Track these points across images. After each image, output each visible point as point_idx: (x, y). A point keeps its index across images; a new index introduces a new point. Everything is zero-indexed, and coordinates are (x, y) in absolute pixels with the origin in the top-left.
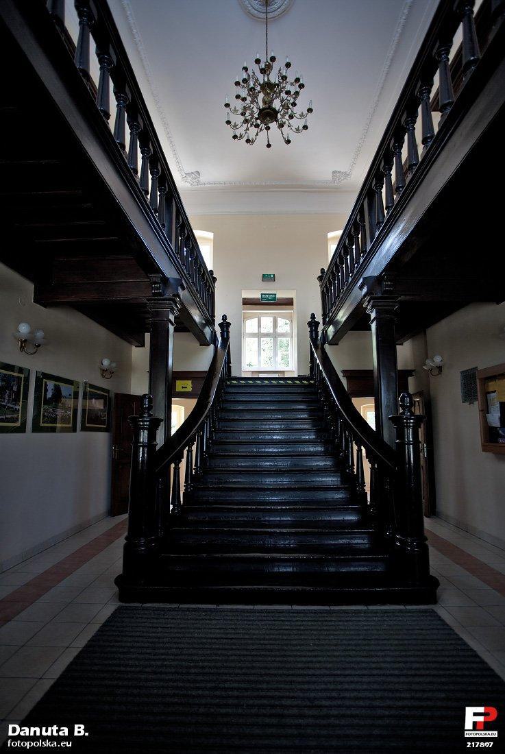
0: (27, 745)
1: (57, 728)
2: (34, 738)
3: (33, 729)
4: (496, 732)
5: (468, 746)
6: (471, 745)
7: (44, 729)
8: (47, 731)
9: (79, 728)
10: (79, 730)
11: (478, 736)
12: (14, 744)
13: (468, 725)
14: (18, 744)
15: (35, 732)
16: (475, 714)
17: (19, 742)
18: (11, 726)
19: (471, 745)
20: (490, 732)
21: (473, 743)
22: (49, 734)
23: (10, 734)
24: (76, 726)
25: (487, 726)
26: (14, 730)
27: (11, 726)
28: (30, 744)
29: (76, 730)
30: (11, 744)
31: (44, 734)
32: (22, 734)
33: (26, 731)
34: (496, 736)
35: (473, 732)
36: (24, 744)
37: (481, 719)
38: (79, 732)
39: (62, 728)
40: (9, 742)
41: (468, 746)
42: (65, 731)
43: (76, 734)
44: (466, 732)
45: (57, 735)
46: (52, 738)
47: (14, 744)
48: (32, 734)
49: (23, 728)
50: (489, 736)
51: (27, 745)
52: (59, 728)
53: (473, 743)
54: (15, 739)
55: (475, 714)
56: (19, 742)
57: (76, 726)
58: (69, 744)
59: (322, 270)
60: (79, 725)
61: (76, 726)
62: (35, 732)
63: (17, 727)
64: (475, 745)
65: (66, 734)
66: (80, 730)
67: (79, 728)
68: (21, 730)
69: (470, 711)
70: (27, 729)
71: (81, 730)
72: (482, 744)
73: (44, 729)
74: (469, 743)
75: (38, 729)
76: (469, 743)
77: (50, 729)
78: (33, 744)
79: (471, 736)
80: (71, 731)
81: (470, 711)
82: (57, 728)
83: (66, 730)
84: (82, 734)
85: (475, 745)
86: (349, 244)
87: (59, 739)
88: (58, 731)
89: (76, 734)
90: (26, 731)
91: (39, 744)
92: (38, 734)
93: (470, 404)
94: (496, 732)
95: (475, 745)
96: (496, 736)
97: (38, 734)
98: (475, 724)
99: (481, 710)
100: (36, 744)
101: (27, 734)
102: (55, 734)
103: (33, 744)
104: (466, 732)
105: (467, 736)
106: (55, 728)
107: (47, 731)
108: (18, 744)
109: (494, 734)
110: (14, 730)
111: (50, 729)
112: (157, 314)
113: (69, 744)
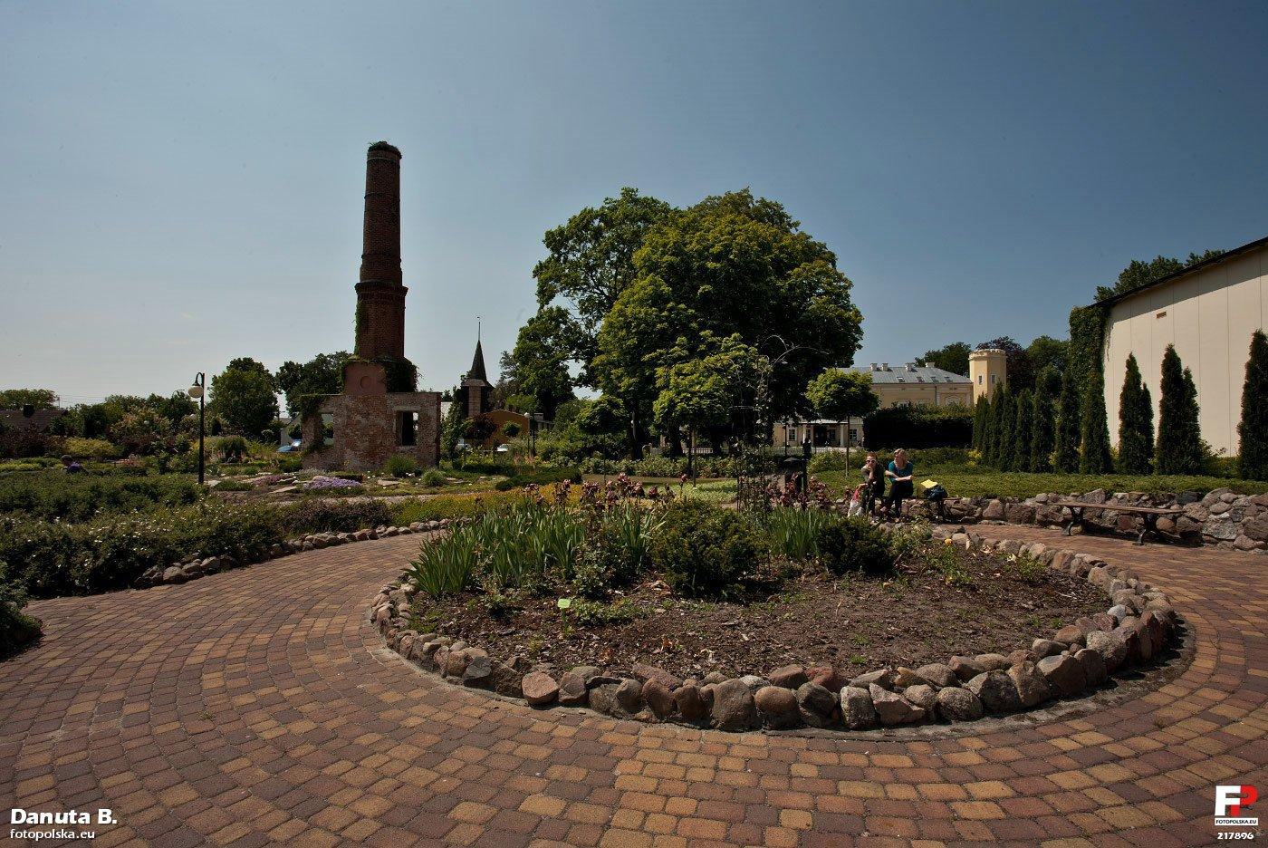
1: (76, 814)
2: (45, 826)
3: (43, 815)
4: (1257, 819)
6: (1224, 836)
7: (58, 815)
9: (105, 813)
10: (105, 816)
11: (1232, 824)
13: (1220, 810)
15: (46, 819)
16: (1229, 796)
17: (25, 832)
18: (14, 812)
19: (1224, 836)
20: (1249, 819)
21: (1226, 834)
22: (65, 821)
23: (14, 821)
24: (101, 811)
27: (14, 812)
28: (40, 835)
29: (101, 816)
30: (14, 834)
31: (58, 821)
32: (29, 821)
33: (34, 818)
34: (1257, 824)
36: (32, 835)
37: (1236, 802)
38: (105, 819)
39: (82, 814)
40: (12, 832)
42: (86, 818)
43: (100, 821)
44: (1216, 819)
45: (75, 822)
46: (68, 827)
47: (19, 835)
48: (42, 822)
49: (30, 814)
50: (1246, 824)
51: (36, 835)
52: (78, 815)
53: (1226, 834)
55: (1229, 796)
56: (25, 832)
57: (101, 811)
58: (91, 835)
59: (506, 353)
62: (46, 819)
64: (1229, 836)
65: (88, 822)
66: (105, 816)
67: (105, 813)
68: (27, 817)
69: (1221, 791)
70: (35, 815)
71: (107, 816)
72: (1238, 834)
73: (58, 815)
75: (50, 815)
76: (1221, 834)
77: (66, 815)
79: (1223, 824)
81: (1221, 791)
82: (76, 814)
83: (87, 816)
85: (1229, 836)
86: (712, 254)
87: (76, 828)
88: (76, 818)
89: (100, 821)
90: (34, 818)
92: (50, 821)
94: (1257, 819)
95: (1229, 836)
96: (1257, 824)
97: (50, 821)
98: (1228, 808)
99: (1236, 789)
100: (48, 835)
101: (36, 822)
102: (73, 821)
104: (1216, 819)
105: (1218, 824)
106: (73, 813)
109: (1253, 821)
110: (18, 816)
111: (66, 815)
113: (91, 835)
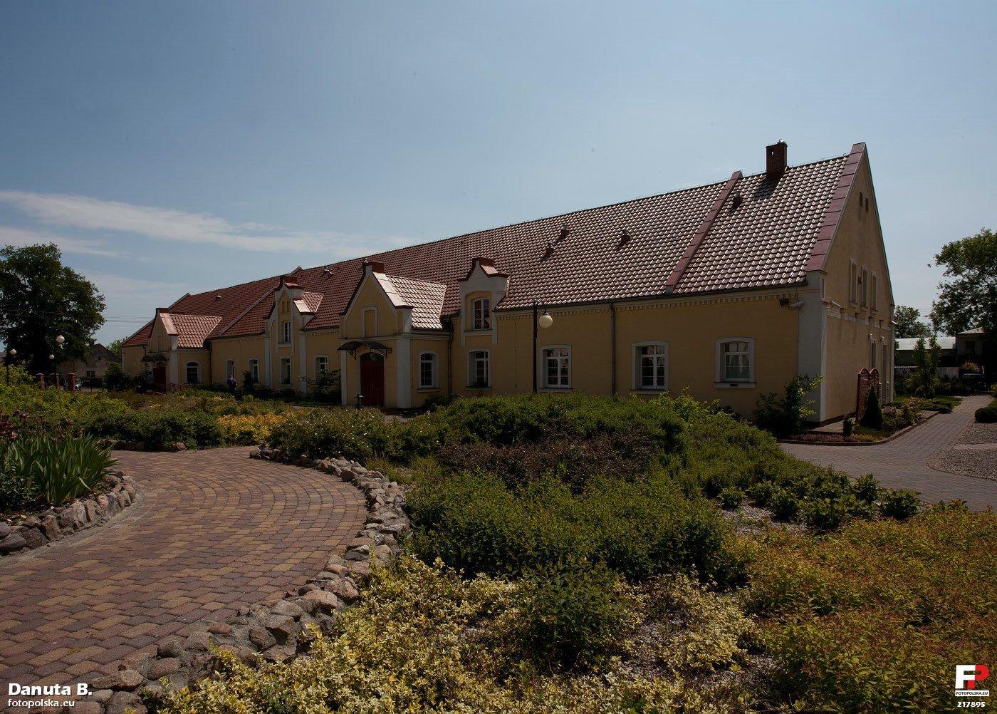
0: (28, 704)
3: (34, 688)
4: (988, 691)
5: (959, 706)
6: (962, 704)
7: (46, 688)
8: (48, 690)
9: (82, 687)
10: (82, 689)
12: (15, 704)
13: (959, 684)
14: (18, 703)
16: (966, 673)
17: (20, 701)
18: (11, 685)
19: (962, 704)
20: (982, 691)
22: (51, 693)
23: (11, 693)
25: (977, 685)
26: (15, 689)
27: (11, 685)
28: (31, 704)
29: (79, 689)
30: (11, 703)
31: (46, 693)
32: (23, 693)
33: (27, 690)
34: (988, 695)
35: (964, 691)
37: (972, 677)
38: (82, 691)
39: (64, 687)
40: (9, 702)
41: (959, 706)
44: (956, 691)
45: (59, 694)
46: (53, 697)
47: (15, 704)
48: (33, 693)
49: (24, 687)
54: (16, 698)
55: (966, 673)
57: (79, 685)
58: (71, 704)
60: (82, 684)
61: (79, 685)
63: (18, 686)
65: (69, 693)
67: (82, 687)
69: (960, 669)
70: (28, 688)
71: (85, 689)
72: (973, 703)
74: (960, 703)
75: (39, 688)
76: (960, 703)
78: (34, 704)
80: (74, 691)
81: (960, 669)
82: (59, 687)
83: (68, 689)
84: (85, 693)
89: (79, 693)
90: (27, 690)
91: (41, 704)
92: (39, 693)
93: (946, 247)
96: (988, 695)
97: (39, 693)
98: (966, 682)
99: (972, 668)
101: (28, 694)
103: (34, 704)
106: (57, 687)
107: (48, 690)
108: (18, 703)
109: (985, 693)
110: (15, 689)
111: (52, 688)
112: (966, 253)
113: (71, 704)
